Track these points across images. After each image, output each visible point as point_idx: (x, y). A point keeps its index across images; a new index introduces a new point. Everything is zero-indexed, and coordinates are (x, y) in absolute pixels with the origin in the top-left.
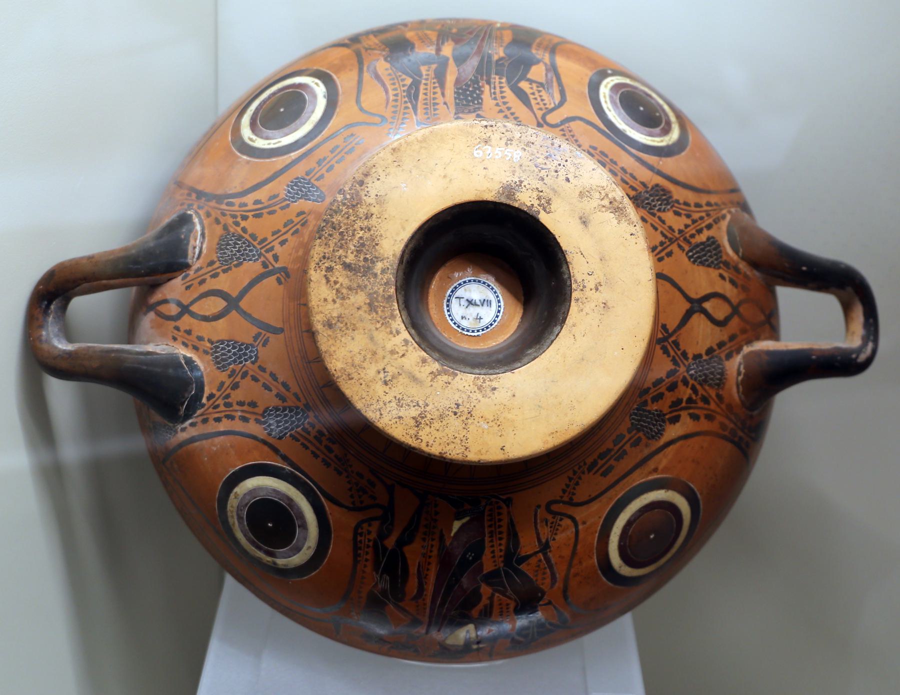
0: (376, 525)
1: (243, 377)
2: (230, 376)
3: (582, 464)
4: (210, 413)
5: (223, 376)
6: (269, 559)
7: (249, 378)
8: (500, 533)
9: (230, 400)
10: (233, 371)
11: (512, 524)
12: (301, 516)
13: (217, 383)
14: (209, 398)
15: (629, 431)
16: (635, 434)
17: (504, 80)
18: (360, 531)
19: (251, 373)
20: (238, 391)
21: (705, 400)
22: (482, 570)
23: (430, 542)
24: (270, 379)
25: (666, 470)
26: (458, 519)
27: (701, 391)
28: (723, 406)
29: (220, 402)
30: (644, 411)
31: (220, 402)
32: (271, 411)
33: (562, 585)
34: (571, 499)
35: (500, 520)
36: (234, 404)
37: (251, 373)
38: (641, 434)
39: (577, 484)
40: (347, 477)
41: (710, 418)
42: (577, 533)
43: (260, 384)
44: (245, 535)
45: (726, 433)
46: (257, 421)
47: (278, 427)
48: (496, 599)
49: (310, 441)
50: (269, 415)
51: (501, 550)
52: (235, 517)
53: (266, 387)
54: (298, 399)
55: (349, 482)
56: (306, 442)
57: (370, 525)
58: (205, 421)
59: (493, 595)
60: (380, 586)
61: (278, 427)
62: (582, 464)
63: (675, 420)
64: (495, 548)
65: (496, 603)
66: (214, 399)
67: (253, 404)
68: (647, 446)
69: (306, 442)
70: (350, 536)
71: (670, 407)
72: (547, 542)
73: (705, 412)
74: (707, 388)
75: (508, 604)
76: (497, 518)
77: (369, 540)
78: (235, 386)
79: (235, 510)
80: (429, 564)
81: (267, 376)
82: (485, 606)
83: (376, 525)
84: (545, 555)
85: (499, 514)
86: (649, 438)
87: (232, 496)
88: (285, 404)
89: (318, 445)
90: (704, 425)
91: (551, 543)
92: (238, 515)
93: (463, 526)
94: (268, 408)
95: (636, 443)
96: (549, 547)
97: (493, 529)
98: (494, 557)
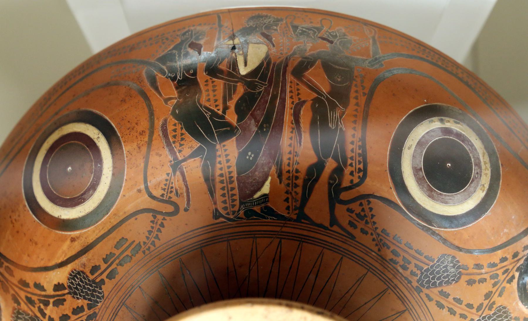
0: (346, 183)
1: (482, 305)
2: (494, 303)
3: (147, 252)
4: (511, 264)
5: (499, 301)
6: (448, 125)
7: (475, 306)
8: (222, 182)
9: (493, 281)
10: (490, 309)
11: (212, 192)
12: (419, 181)
13: (505, 294)
14: (513, 277)
15: (102, 282)
16: (96, 278)
17: (253, 156)
18: (361, 174)
19: (474, 311)
20: (485, 291)
21: (30, 301)
22: (237, 138)
23: (291, 169)
24: (455, 309)
25: (63, 239)
26: (265, 195)
27: (36, 310)
28: (12, 292)
29: (501, 277)
30: (90, 300)
31: (501, 277)
32: (453, 280)
33: (156, 121)
34: (155, 217)
35: (223, 195)
36: (488, 278)
37: (474, 311)
38: (91, 277)
39: (150, 232)
40: (376, 228)
41: (24, 284)
42: (146, 181)
43: (465, 303)
44: (472, 145)
45: (6, 264)
46: (466, 268)
47: (446, 267)
48: (221, 107)
49: (414, 258)
50: (455, 276)
51: (220, 163)
52: (482, 164)
53: (458, 301)
54: (427, 296)
55: (374, 223)
56: (418, 256)
57: (352, 181)
58: (515, 255)
59: (224, 112)
60: (338, 114)
61: (446, 267)
62: (147, 252)
63: (58, 287)
64: (226, 165)
65: (220, 102)
66: (508, 278)
67: (470, 283)
68: (84, 265)
69: (418, 256)
70: (370, 168)
71: (65, 300)
72: (174, 172)
73: (29, 290)
74: (30, 313)
75: (209, 100)
76: (227, 198)
77: (351, 165)
78: (488, 296)
79: (484, 172)
80: (290, 145)
81: (459, 311)
82: (231, 98)
83: (346, 183)
84: (176, 158)
85: (225, 202)
86: (82, 272)
87: (487, 186)
88: (440, 289)
89: (406, 256)
90: (30, 278)
91: (170, 171)
92: (480, 167)
93: (259, 189)
94: (457, 282)
95: (95, 269)
96: (171, 166)
97: (230, 186)
98: (227, 155)
